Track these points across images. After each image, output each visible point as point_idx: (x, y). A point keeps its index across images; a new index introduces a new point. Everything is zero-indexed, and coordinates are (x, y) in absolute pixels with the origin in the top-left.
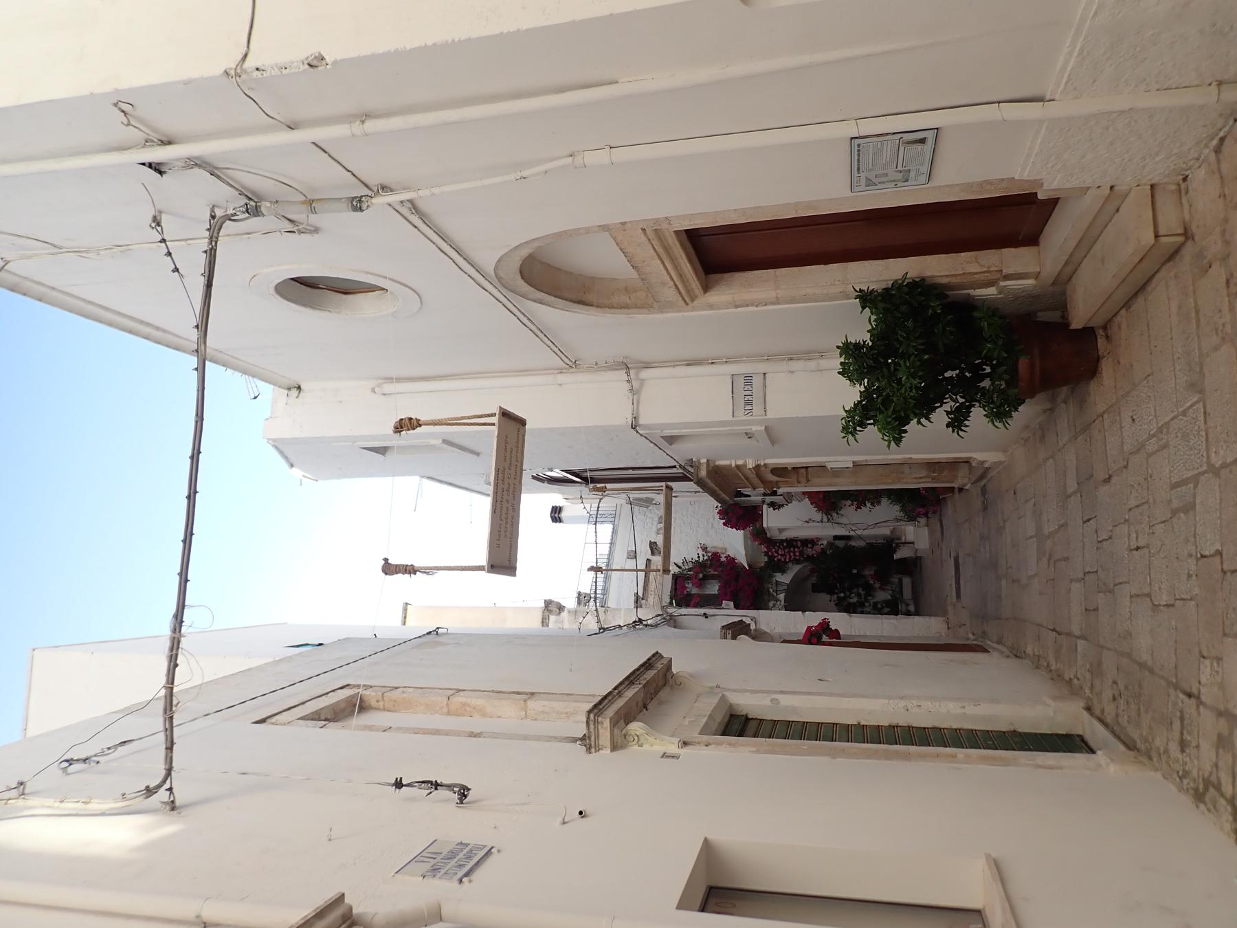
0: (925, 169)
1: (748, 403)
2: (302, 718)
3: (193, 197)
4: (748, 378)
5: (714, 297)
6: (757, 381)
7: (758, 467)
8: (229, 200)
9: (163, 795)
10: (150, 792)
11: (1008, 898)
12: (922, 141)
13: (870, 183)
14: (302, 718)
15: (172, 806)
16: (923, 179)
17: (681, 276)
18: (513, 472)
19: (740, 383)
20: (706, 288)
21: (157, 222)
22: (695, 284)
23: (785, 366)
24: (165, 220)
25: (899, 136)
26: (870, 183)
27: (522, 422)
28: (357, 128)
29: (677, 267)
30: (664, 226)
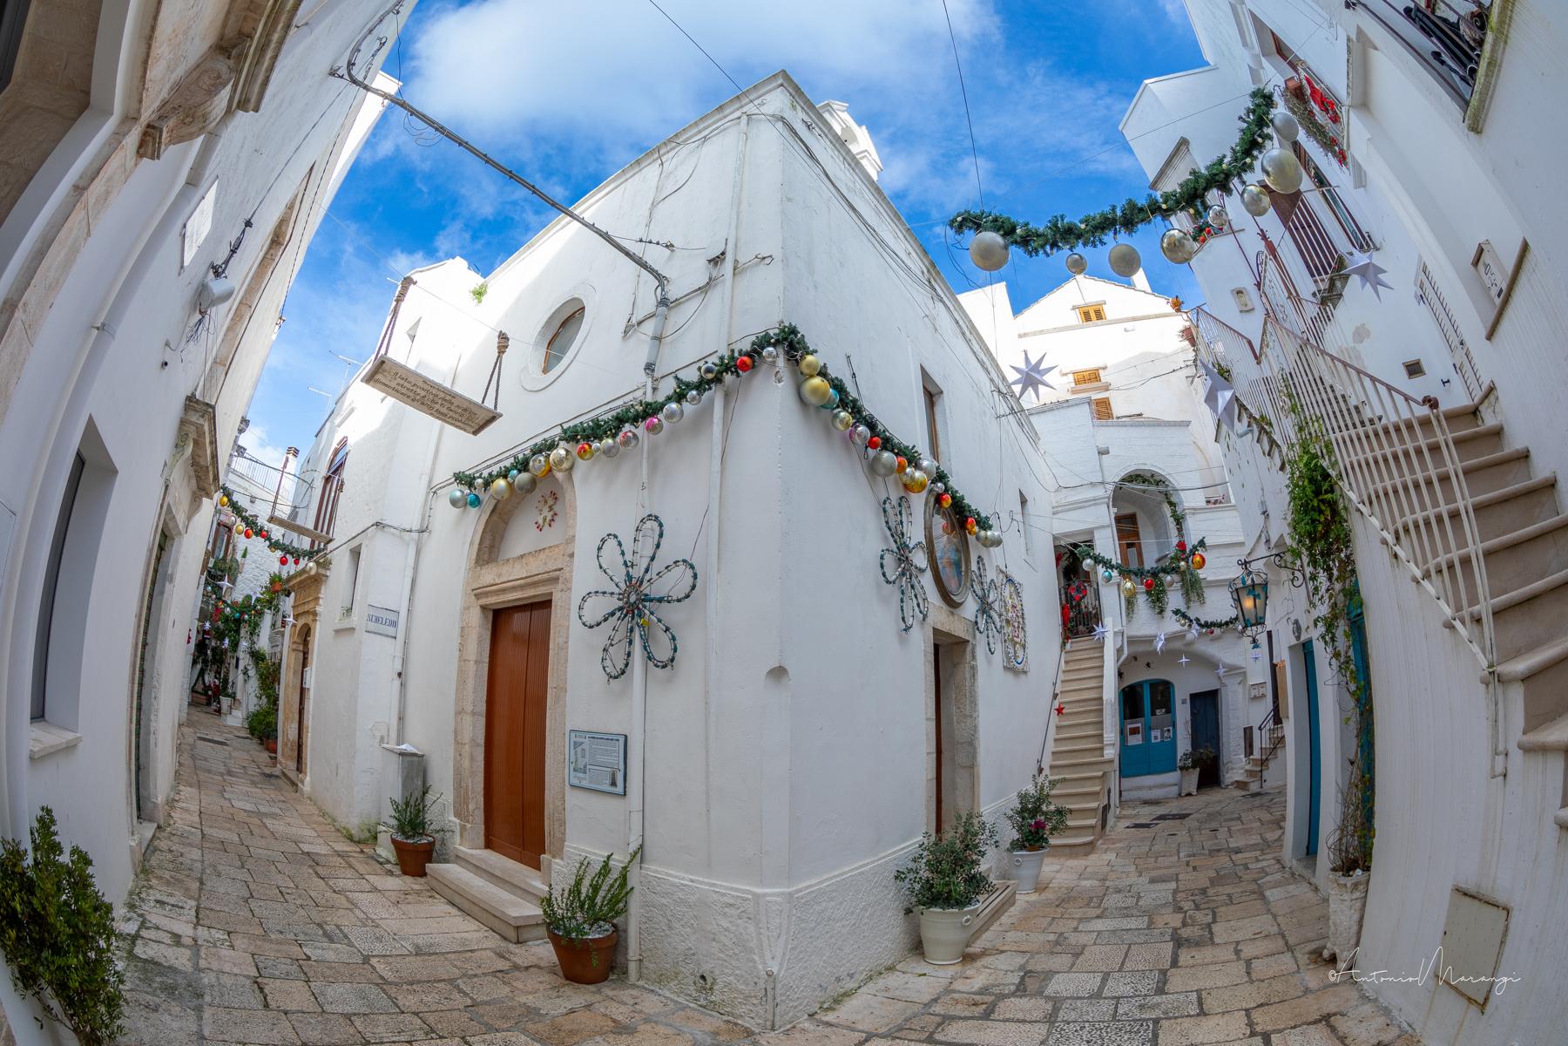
0: (585, 784)
1: (377, 620)
2: (1342, 158)
3: (686, 274)
4: (394, 624)
5: (476, 613)
6: (391, 630)
7: (315, 614)
8: (674, 292)
9: (343, 71)
10: (351, 64)
11: (142, 671)
12: (614, 784)
13: (576, 745)
14: (1342, 158)
15: (333, 73)
16: (575, 782)
17: (504, 591)
18: (444, 410)
19: (392, 617)
20: (484, 608)
21: (669, 246)
22: (492, 600)
23: (399, 654)
24: (667, 252)
25: (622, 767)
26: (576, 745)
27: (475, 433)
28: (334, 445)
29: (514, 589)
30: (560, 586)
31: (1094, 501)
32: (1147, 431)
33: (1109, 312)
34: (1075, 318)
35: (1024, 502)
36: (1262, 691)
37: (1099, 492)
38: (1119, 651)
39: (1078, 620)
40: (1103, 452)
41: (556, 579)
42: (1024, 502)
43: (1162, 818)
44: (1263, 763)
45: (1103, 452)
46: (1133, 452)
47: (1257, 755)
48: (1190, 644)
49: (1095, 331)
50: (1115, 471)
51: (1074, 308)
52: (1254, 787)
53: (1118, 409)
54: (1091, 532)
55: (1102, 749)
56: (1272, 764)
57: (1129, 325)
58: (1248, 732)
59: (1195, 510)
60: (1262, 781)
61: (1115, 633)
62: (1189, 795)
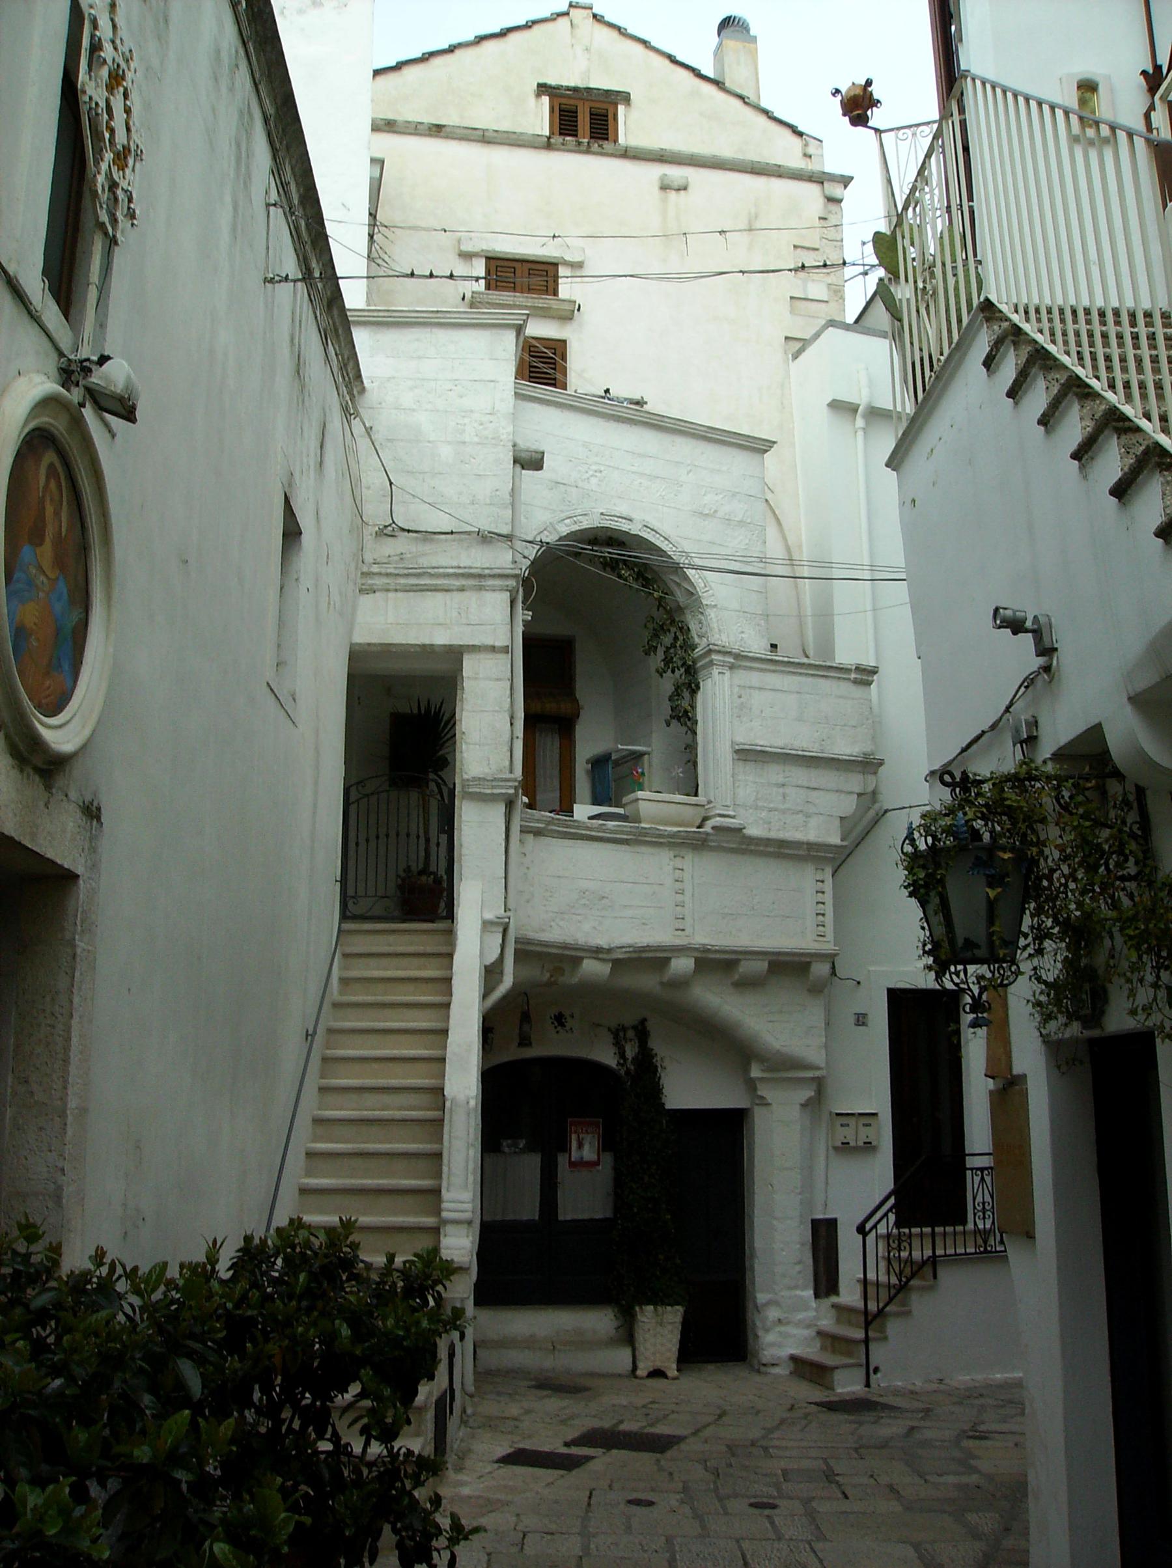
31: (477, 579)
32: (650, 441)
33: (631, 128)
34: (538, 118)
35: (292, 533)
36: (864, 1134)
37: (501, 559)
38: (491, 973)
39: (399, 872)
40: (530, 461)
41: (875, 673)
42: (292, 533)
43: (605, 1439)
44: (871, 1320)
45: (530, 461)
46: (604, 481)
47: (849, 1294)
48: (680, 983)
49: (579, 170)
50: (553, 511)
51: (543, 89)
52: (848, 1385)
53: (585, 371)
54: (455, 654)
55: (436, 1231)
56: (893, 1327)
57: (676, 173)
58: (824, 1235)
59: (739, 660)
60: (870, 1370)
61: (486, 925)
62: (657, 1373)
